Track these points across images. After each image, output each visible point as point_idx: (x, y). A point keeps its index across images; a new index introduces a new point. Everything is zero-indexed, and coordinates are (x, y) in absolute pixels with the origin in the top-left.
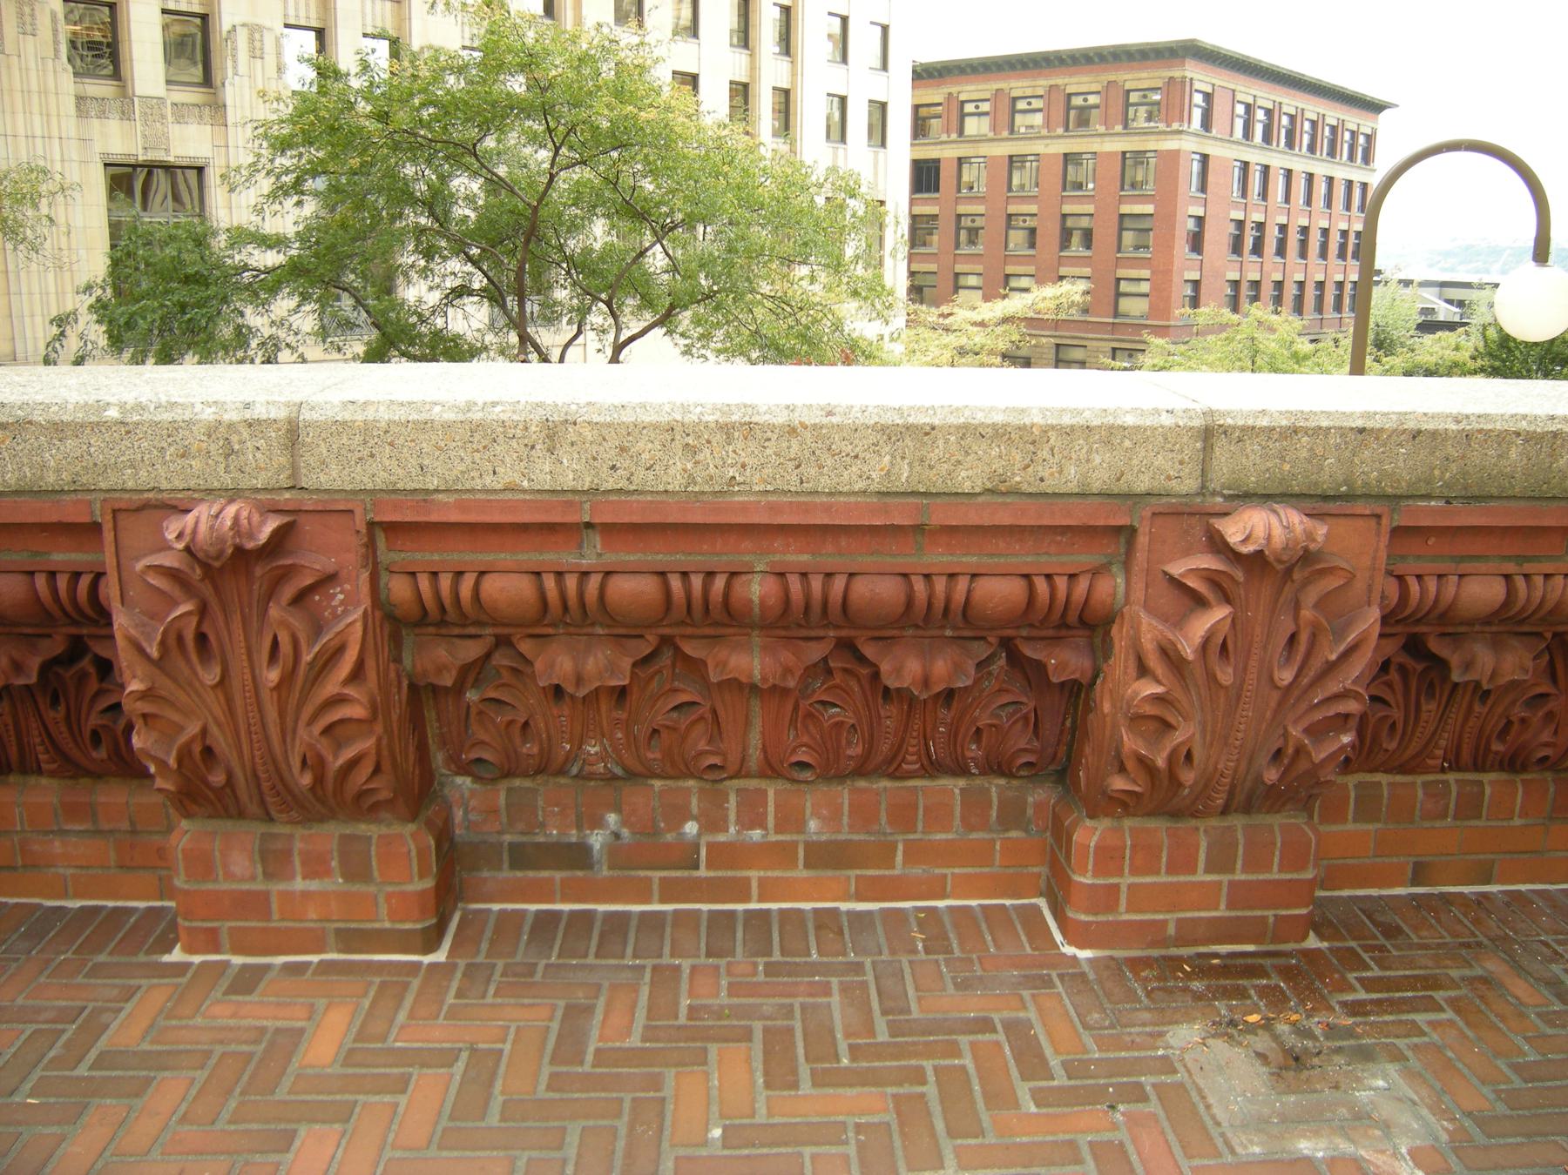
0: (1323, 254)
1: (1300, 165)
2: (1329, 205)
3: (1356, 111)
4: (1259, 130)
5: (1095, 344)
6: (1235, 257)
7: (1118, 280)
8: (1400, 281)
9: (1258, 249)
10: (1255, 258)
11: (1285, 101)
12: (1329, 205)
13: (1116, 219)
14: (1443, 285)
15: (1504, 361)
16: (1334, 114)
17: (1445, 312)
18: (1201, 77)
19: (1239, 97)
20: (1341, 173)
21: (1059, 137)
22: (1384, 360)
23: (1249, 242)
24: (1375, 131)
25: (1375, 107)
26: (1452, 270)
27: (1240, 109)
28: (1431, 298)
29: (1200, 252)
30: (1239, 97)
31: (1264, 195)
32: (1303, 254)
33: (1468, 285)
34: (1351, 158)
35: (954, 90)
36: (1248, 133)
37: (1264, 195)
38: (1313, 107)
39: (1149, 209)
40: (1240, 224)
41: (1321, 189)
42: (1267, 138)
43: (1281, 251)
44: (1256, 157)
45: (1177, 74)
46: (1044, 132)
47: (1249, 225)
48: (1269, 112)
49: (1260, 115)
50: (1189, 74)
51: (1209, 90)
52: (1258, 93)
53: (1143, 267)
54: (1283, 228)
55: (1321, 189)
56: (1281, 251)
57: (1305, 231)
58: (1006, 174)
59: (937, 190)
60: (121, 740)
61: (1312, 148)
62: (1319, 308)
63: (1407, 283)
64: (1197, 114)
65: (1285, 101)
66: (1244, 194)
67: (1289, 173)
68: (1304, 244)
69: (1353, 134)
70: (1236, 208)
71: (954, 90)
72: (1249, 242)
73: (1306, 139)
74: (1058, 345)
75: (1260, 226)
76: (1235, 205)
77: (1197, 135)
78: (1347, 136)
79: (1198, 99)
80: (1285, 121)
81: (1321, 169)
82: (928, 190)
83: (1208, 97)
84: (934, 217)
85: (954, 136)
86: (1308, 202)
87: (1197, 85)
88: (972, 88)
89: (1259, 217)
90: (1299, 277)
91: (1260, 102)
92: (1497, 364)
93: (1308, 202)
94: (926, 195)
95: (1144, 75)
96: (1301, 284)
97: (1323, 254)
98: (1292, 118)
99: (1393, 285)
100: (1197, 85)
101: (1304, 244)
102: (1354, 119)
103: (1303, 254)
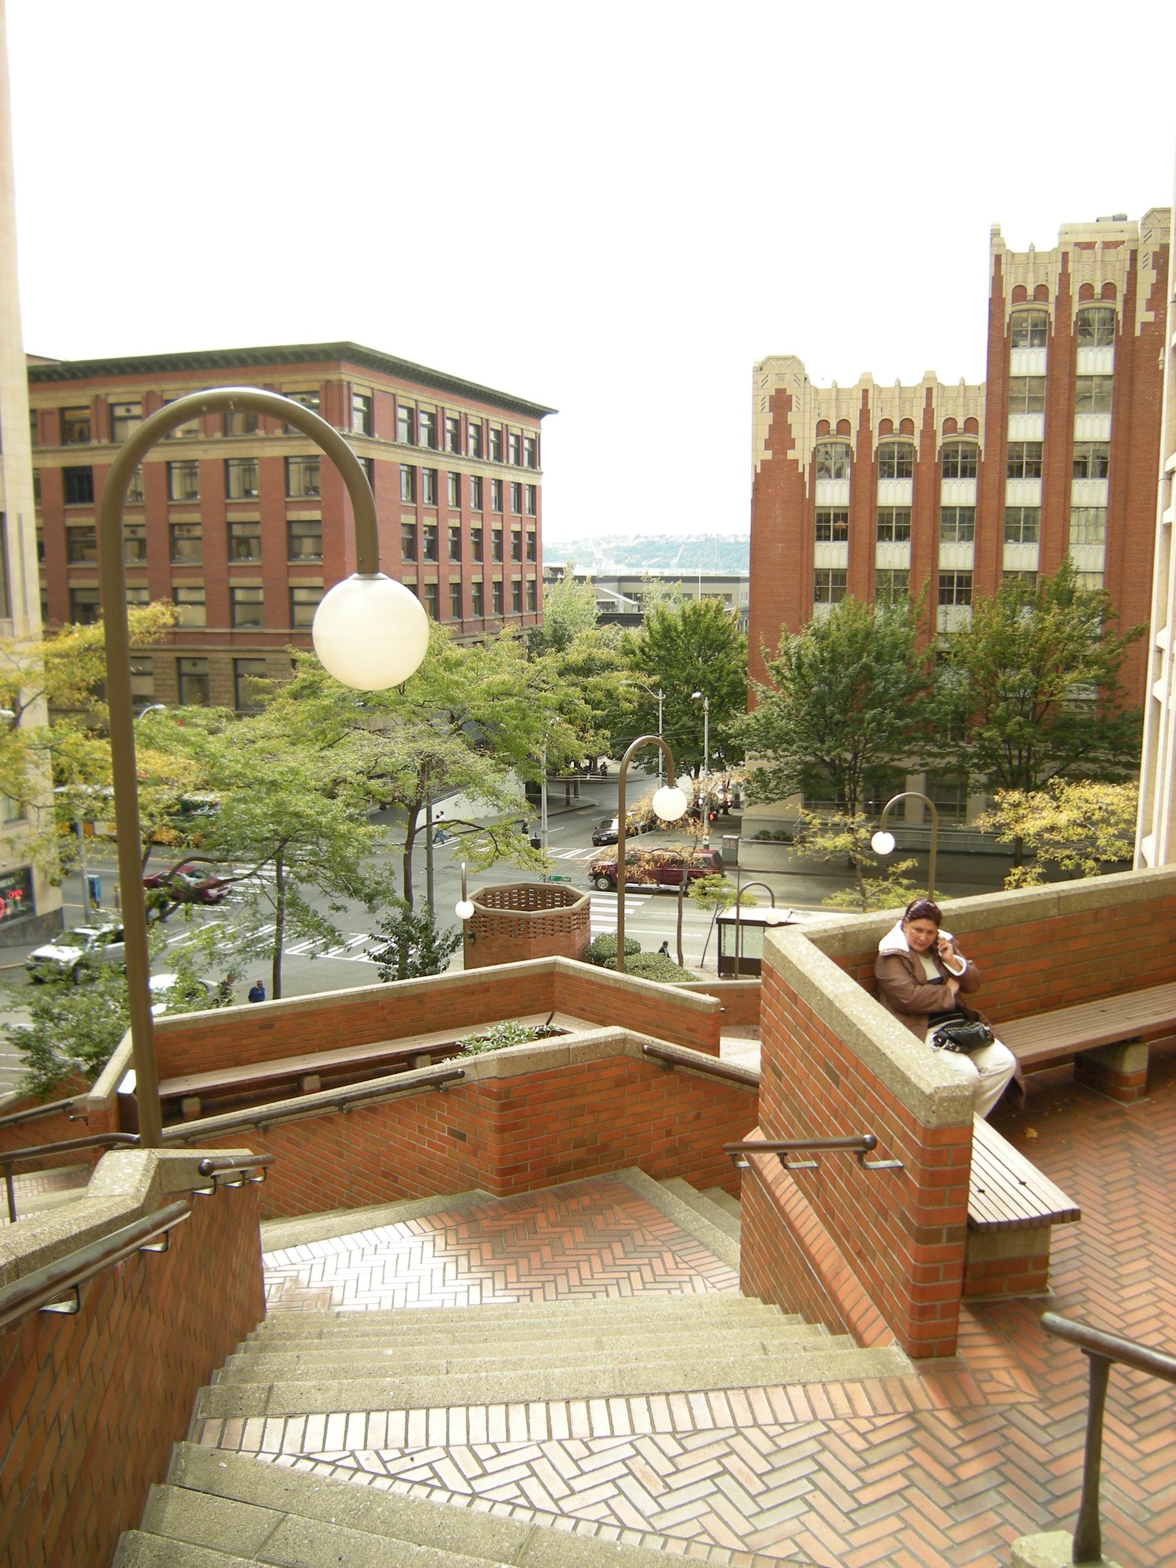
0: (499, 555)
1: (468, 469)
2: (500, 507)
3: (518, 416)
4: (423, 434)
5: (274, 656)
6: (410, 562)
7: (292, 589)
8: (576, 578)
9: (432, 552)
10: (431, 562)
11: (447, 405)
12: (500, 507)
13: (283, 527)
14: (621, 579)
15: (668, 650)
16: (497, 419)
17: (624, 606)
18: (360, 382)
19: (401, 401)
20: (509, 477)
21: (218, 442)
22: (538, 660)
23: (422, 547)
24: (538, 436)
25: (536, 413)
26: (638, 565)
27: (403, 414)
28: (610, 592)
29: (459, 559)
30: (401, 401)
31: (434, 498)
32: (479, 556)
33: (637, 579)
34: (518, 461)
35: (101, 391)
36: (518, 461)
37: (434, 498)
38: (476, 413)
39: (316, 515)
40: (412, 528)
41: (491, 491)
42: (433, 441)
43: (456, 553)
44: (422, 461)
45: (333, 376)
46: (202, 436)
47: (421, 530)
48: (432, 417)
49: (424, 420)
50: (345, 378)
51: (369, 394)
52: (524, 427)
53: (316, 575)
54: (456, 531)
55: (491, 491)
56: (456, 553)
57: (478, 533)
58: (164, 481)
59: (91, 499)
60: (144, 910)
61: (478, 452)
62: (458, 612)
63: (581, 579)
64: (358, 420)
65: (447, 405)
66: (414, 499)
67: (434, 473)
68: (479, 546)
69: (518, 438)
70: (406, 513)
71: (101, 391)
72: (422, 547)
73: (472, 443)
74: (235, 660)
75: (433, 530)
76: (406, 510)
77: (358, 439)
78: (512, 440)
79: (358, 403)
80: (449, 425)
81: (489, 473)
82: (82, 499)
83: (368, 401)
84: (91, 529)
85: (105, 442)
86: (480, 505)
87: (355, 389)
88: (121, 390)
89: (430, 521)
90: (477, 579)
91: (422, 407)
92: (663, 653)
93: (480, 505)
94: (79, 506)
95: (300, 378)
96: (479, 586)
97: (499, 555)
98: (456, 423)
99: (569, 583)
100: (355, 389)
101: (479, 546)
102: (517, 425)
103: (479, 556)
